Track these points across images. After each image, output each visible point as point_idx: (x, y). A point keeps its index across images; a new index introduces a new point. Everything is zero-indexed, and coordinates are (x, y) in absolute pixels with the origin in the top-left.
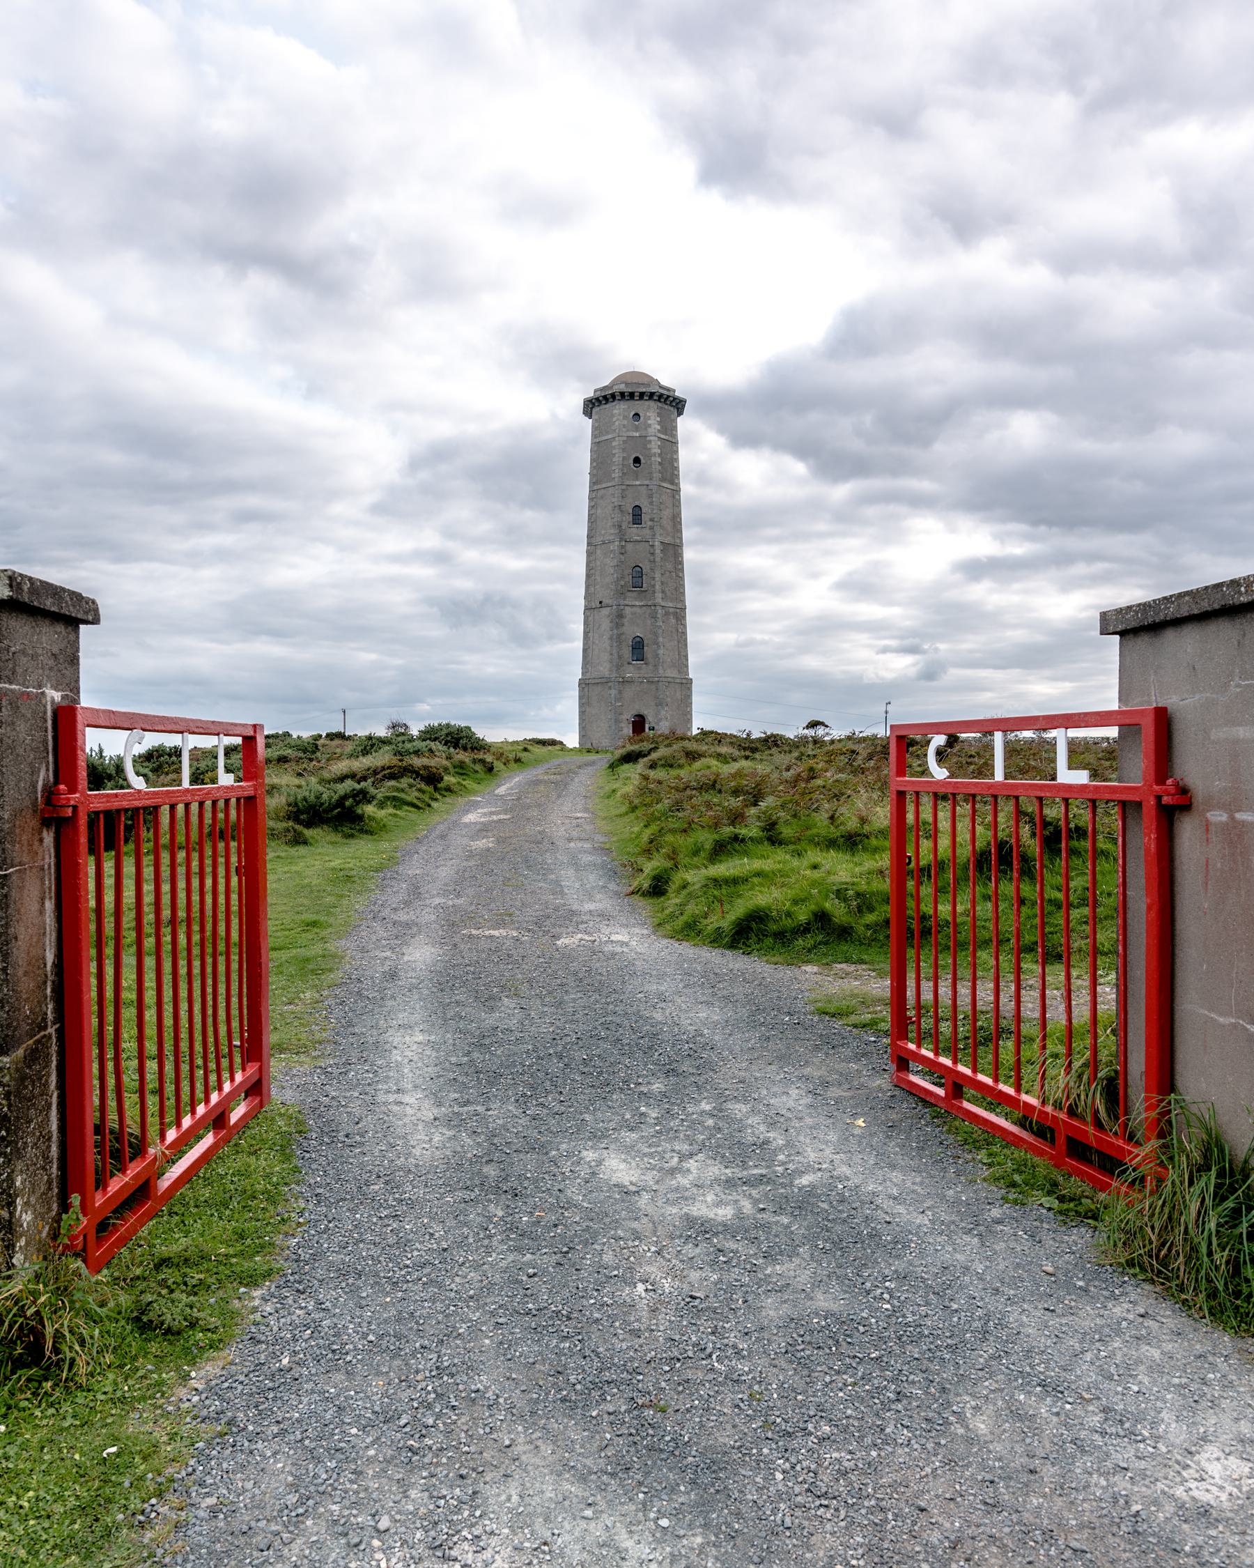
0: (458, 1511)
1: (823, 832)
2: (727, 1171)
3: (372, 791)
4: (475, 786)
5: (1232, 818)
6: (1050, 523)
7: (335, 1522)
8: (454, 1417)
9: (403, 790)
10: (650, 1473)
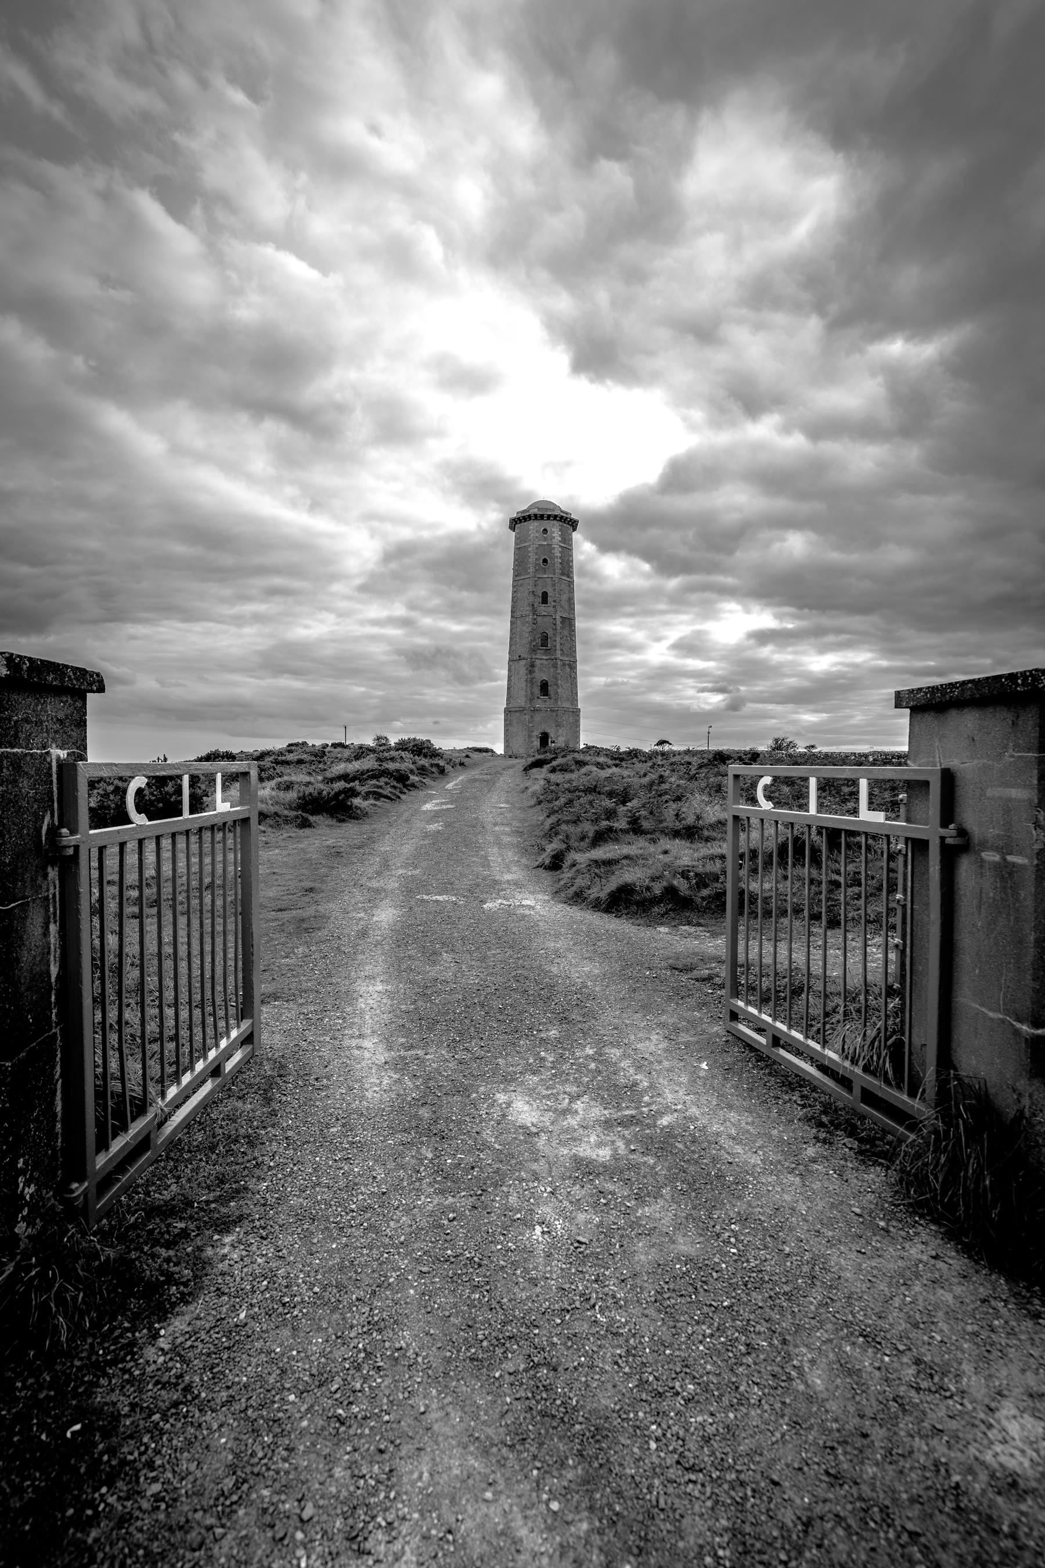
0: (375, 1493)
1: (671, 825)
2: (606, 1112)
3: (359, 788)
4: (432, 783)
5: (1005, 860)
6: (811, 608)
7: (265, 1511)
8: (379, 1380)
9: (381, 787)
10: (543, 1444)
